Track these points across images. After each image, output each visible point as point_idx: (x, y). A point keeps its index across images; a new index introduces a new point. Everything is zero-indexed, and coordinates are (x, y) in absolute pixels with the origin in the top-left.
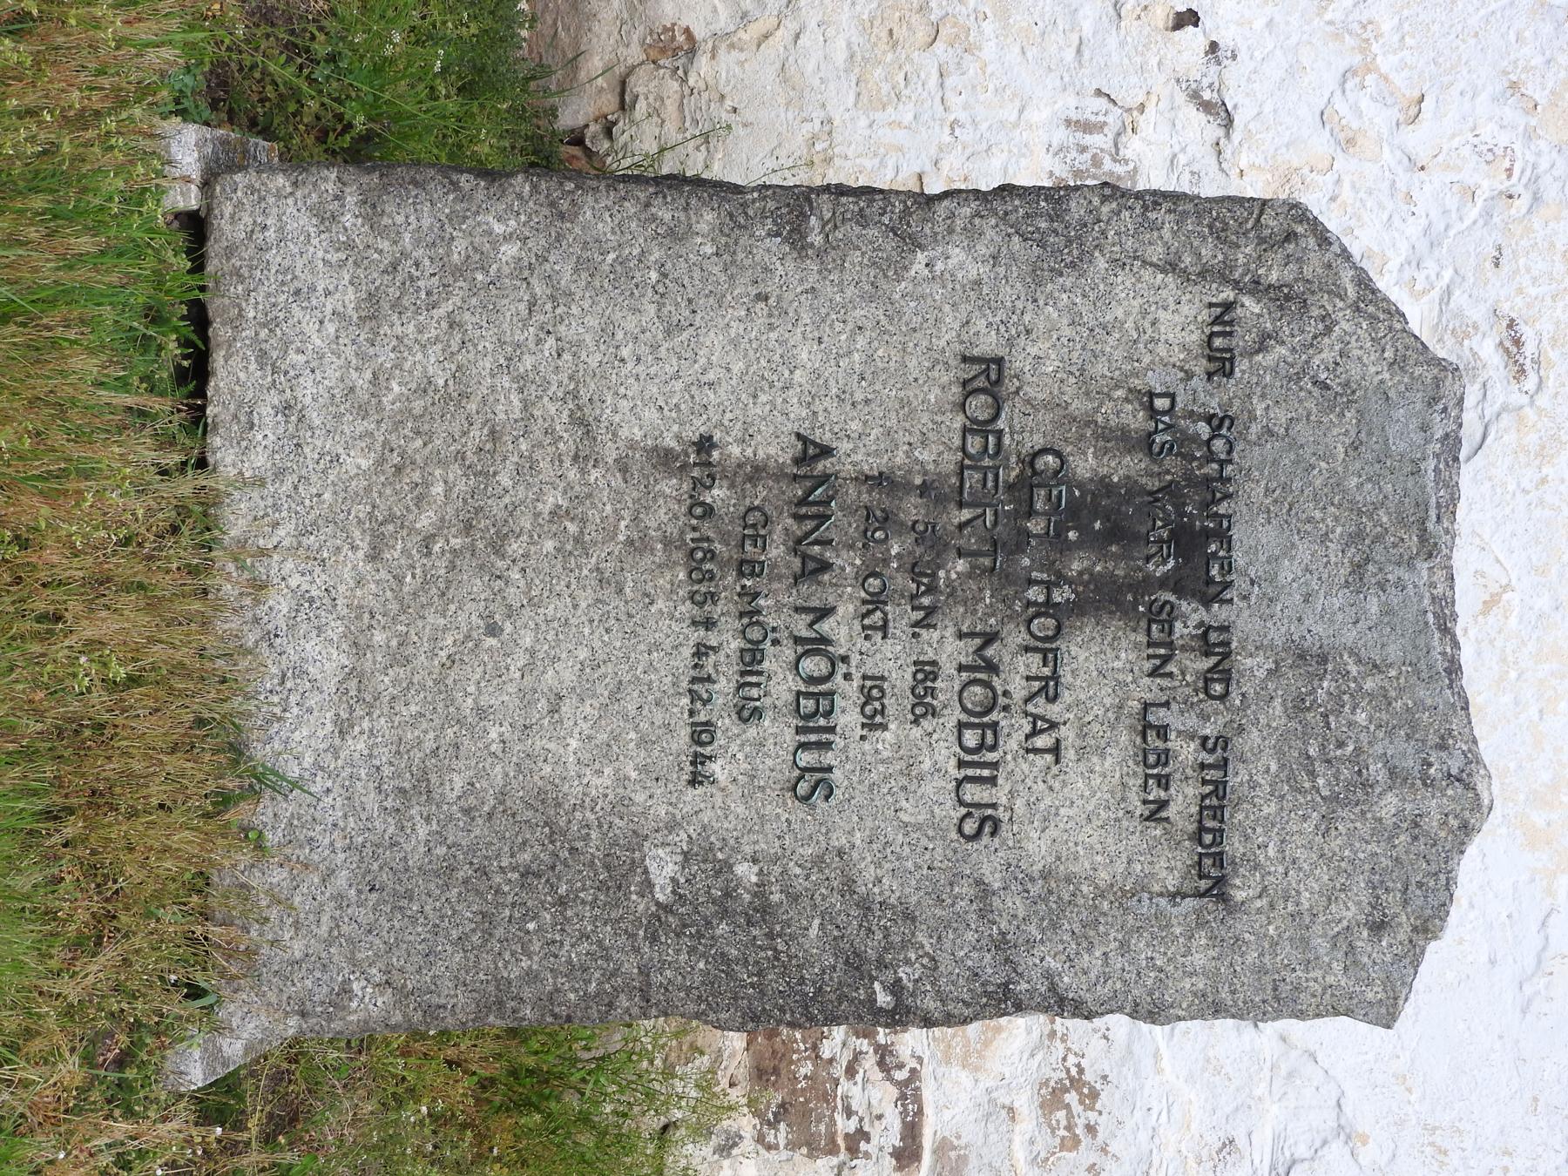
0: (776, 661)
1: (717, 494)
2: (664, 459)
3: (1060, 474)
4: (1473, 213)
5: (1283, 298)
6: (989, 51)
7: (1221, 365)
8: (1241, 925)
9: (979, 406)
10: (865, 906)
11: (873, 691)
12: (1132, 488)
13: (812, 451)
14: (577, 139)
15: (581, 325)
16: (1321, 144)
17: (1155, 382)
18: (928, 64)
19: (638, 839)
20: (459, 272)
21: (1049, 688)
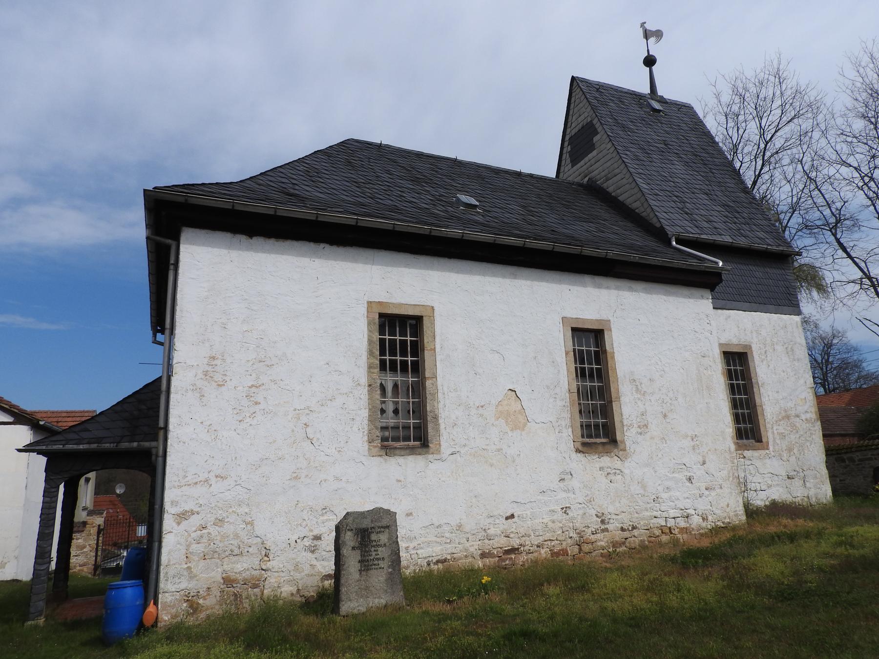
0: (375, 563)
1: (363, 569)
2: (360, 573)
3: (360, 541)
4: (312, 513)
5: (347, 526)
6: (299, 560)
7: (352, 530)
8: (391, 524)
9: (355, 548)
10: (391, 554)
11: (376, 555)
12: (361, 536)
13: (359, 562)
14: (306, 601)
15: (350, 582)
16: (307, 528)
17: (353, 535)
18: (300, 566)
19: (388, 572)
20: (347, 593)
21: (375, 541)
